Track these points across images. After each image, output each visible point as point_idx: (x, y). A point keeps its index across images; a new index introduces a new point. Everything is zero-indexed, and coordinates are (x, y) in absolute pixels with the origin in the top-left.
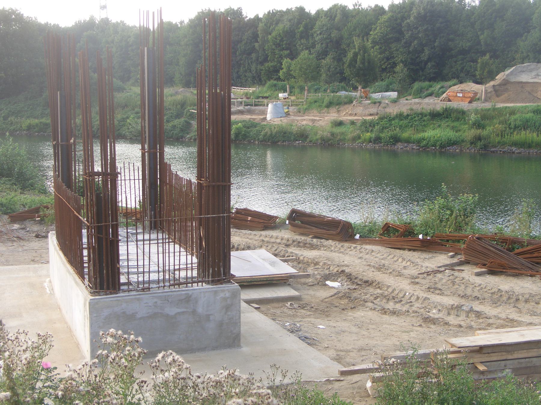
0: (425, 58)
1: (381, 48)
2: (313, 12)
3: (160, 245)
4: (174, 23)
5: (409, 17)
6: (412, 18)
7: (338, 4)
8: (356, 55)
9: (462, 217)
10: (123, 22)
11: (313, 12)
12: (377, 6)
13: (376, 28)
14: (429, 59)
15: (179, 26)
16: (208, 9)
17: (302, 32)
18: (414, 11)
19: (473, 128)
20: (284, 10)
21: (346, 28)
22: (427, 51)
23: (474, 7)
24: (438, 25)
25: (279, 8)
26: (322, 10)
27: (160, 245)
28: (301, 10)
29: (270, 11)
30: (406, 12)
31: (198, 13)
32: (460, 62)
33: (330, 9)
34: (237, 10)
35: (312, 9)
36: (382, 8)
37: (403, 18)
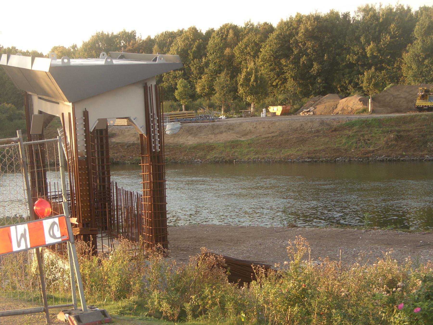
0: (315, 73)
1: (271, 65)
2: (204, 32)
3: (110, 240)
4: (67, 48)
5: (297, 33)
6: (300, 35)
7: (228, 24)
8: (249, 74)
9: (387, 258)
10: (15, 48)
11: (204, 32)
12: (266, 24)
13: (265, 46)
14: (319, 74)
15: (72, 50)
16: (101, 32)
17: (195, 52)
18: (302, 29)
19: (280, 41)
20: (176, 31)
21: (237, 46)
22: (316, 66)
23: (358, 22)
24: (326, 40)
25: (170, 30)
26: (213, 30)
27: (110, 240)
28: (194, 31)
29: (163, 33)
30: (293, 29)
31: (93, 36)
32: (348, 75)
33: (221, 29)
34: (131, 33)
35: (203, 30)
36: (271, 26)
37: (291, 35)
